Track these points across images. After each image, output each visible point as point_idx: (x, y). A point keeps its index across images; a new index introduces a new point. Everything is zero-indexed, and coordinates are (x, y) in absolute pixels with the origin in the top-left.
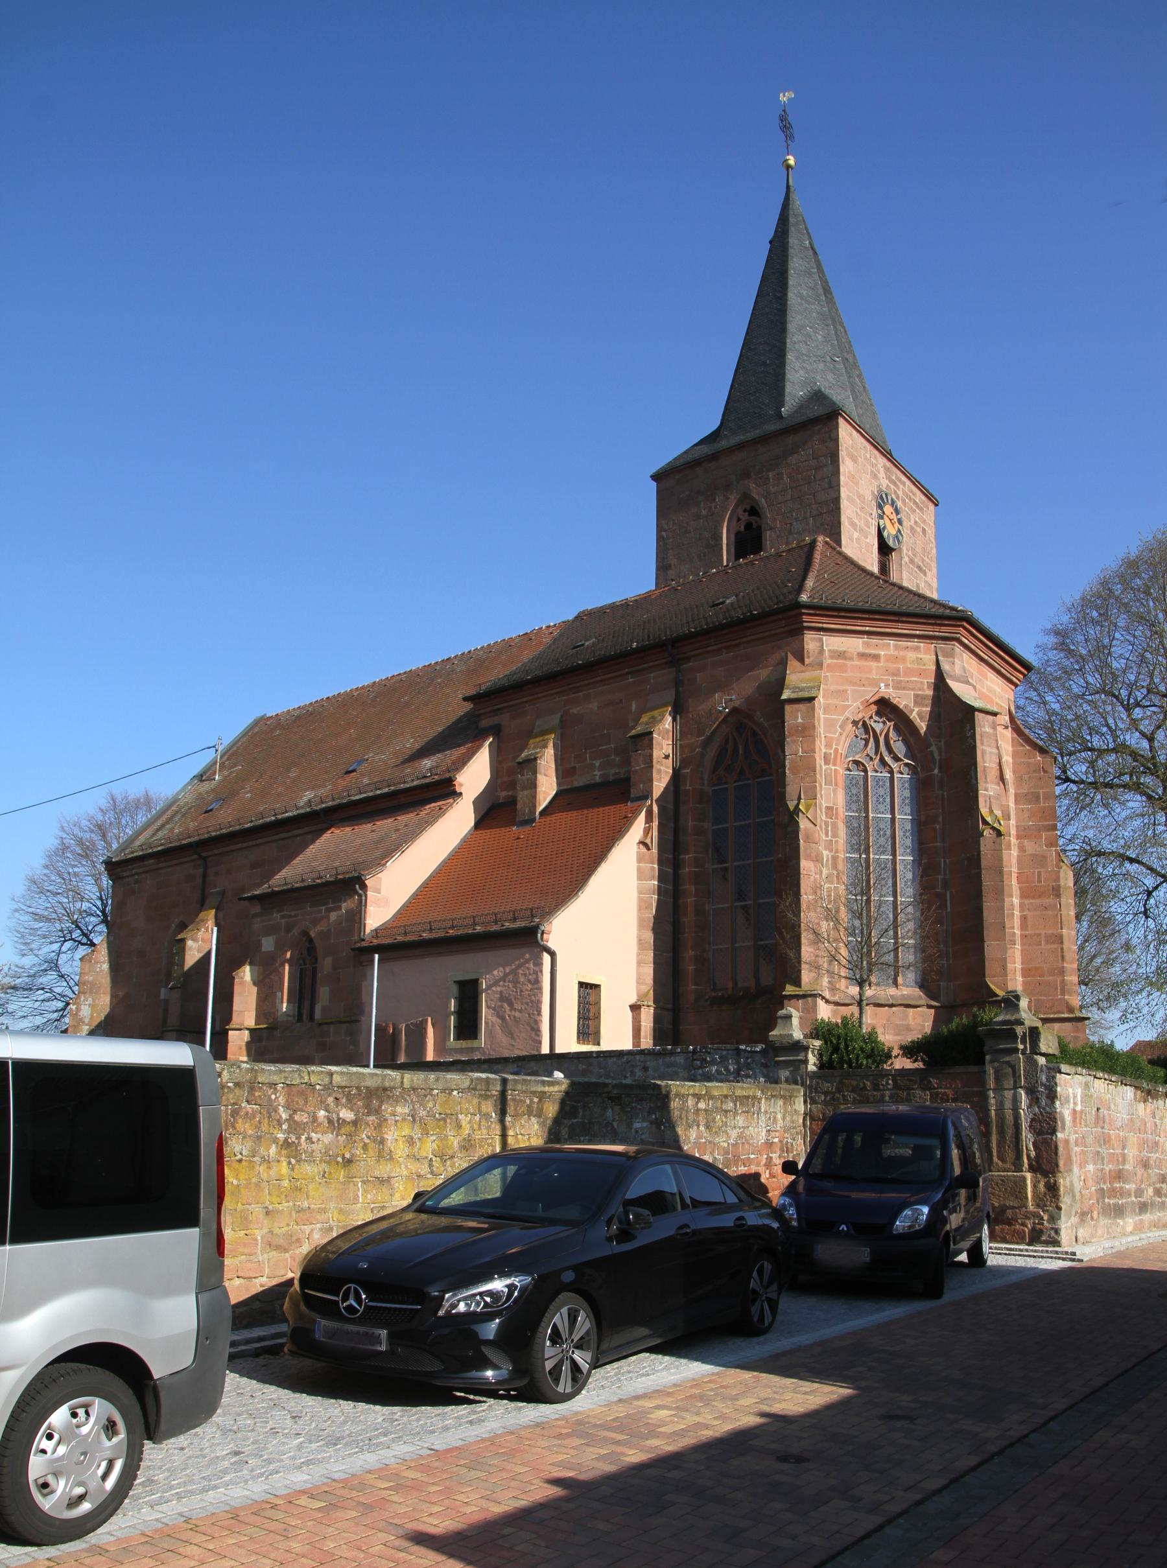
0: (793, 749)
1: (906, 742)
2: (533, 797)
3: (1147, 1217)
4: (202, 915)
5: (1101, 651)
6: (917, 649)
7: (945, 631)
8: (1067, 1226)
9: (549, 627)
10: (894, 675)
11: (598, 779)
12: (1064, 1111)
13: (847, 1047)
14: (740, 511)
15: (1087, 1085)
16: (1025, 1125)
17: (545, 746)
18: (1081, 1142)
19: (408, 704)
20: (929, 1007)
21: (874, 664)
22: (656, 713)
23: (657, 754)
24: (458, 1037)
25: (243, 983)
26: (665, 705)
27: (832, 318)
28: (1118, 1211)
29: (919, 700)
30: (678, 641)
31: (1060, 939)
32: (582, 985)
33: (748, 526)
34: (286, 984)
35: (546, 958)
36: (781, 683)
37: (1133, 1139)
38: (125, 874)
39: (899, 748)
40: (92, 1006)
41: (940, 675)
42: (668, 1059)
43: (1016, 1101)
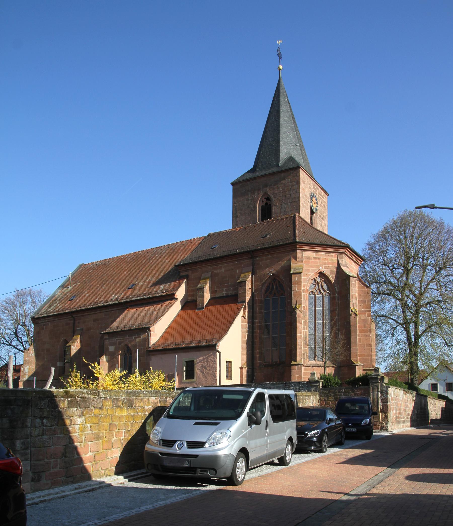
0: (294, 289)
1: (327, 285)
2: (203, 300)
3: (405, 424)
4: (75, 337)
5: (383, 252)
6: (332, 256)
7: (341, 250)
8: (389, 425)
9: (197, 238)
10: (325, 264)
11: (225, 295)
12: (390, 397)
13: (330, 382)
14: (263, 199)
15: (394, 391)
16: (380, 401)
17: (206, 283)
18: (393, 405)
19: (146, 264)
20: (333, 367)
21: (318, 261)
22: (246, 274)
23: (247, 288)
24: (186, 378)
25: (103, 361)
26: (250, 272)
27: (296, 129)
28: (399, 422)
29: (332, 272)
30: (253, 251)
31: (371, 345)
32: (227, 362)
33: (266, 204)
34: (120, 362)
35: (218, 354)
36: (289, 267)
37: (403, 404)
38: (39, 322)
39: (325, 287)
40: (29, 369)
41: (339, 265)
42: (277, 385)
43: (377, 395)
